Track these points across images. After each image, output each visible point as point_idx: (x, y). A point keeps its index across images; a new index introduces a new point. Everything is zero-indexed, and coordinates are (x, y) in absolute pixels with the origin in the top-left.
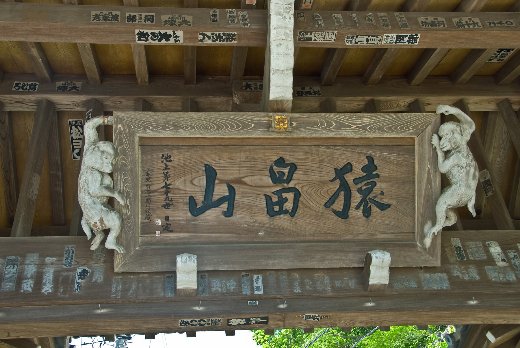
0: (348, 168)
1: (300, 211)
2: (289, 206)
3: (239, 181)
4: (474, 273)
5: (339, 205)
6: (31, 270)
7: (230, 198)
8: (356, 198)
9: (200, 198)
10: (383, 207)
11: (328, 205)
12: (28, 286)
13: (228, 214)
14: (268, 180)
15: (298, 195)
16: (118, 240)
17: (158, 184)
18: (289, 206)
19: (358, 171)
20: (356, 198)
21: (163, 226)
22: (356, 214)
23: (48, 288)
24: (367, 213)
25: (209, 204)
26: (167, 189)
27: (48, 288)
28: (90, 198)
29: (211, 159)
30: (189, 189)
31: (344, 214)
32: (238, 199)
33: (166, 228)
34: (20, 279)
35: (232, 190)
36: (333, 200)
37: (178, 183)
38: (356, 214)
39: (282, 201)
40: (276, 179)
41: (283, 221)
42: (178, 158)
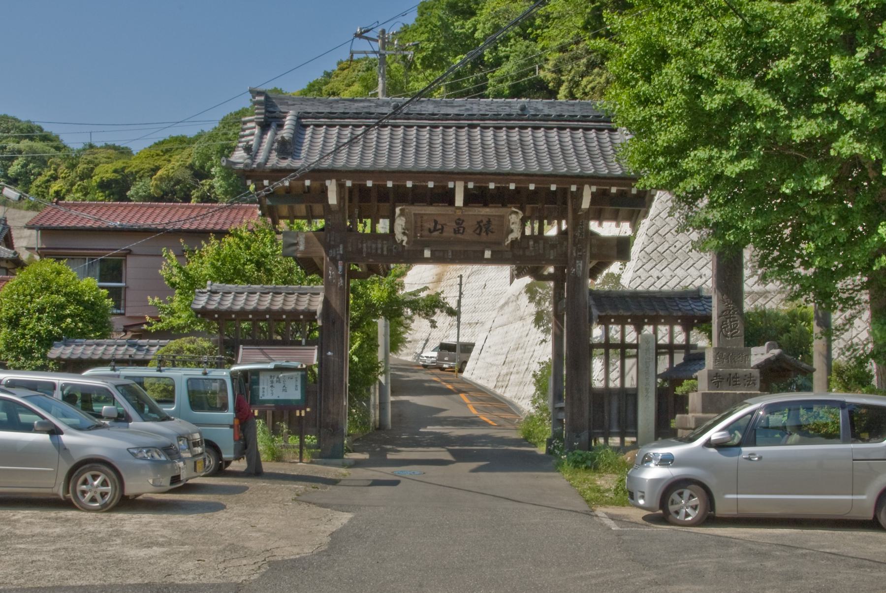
0: (482, 221)
1: (465, 233)
2: (461, 231)
3: (445, 224)
4: (521, 253)
5: (478, 231)
6: (380, 246)
7: (442, 229)
8: (484, 230)
9: (432, 229)
10: (492, 232)
11: (474, 231)
12: (374, 251)
13: (442, 233)
14: (455, 224)
15: (464, 228)
16: (407, 243)
17: (419, 224)
18: (461, 231)
19: (485, 222)
20: (484, 230)
21: (447, 192)
22: (484, 234)
23: (385, 253)
24: (487, 234)
25: (435, 230)
26: (422, 226)
27: (385, 253)
28: (421, 281)
29: (435, 218)
30: (429, 226)
31: (479, 234)
32: (445, 229)
33: (421, 236)
34: (377, 249)
35: (443, 227)
36: (476, 230)
37: (425, 224)
38: (484, 234)
39: (459, 230)
40: (457, 224)
41: (459, 236)
42: (425, 218)
